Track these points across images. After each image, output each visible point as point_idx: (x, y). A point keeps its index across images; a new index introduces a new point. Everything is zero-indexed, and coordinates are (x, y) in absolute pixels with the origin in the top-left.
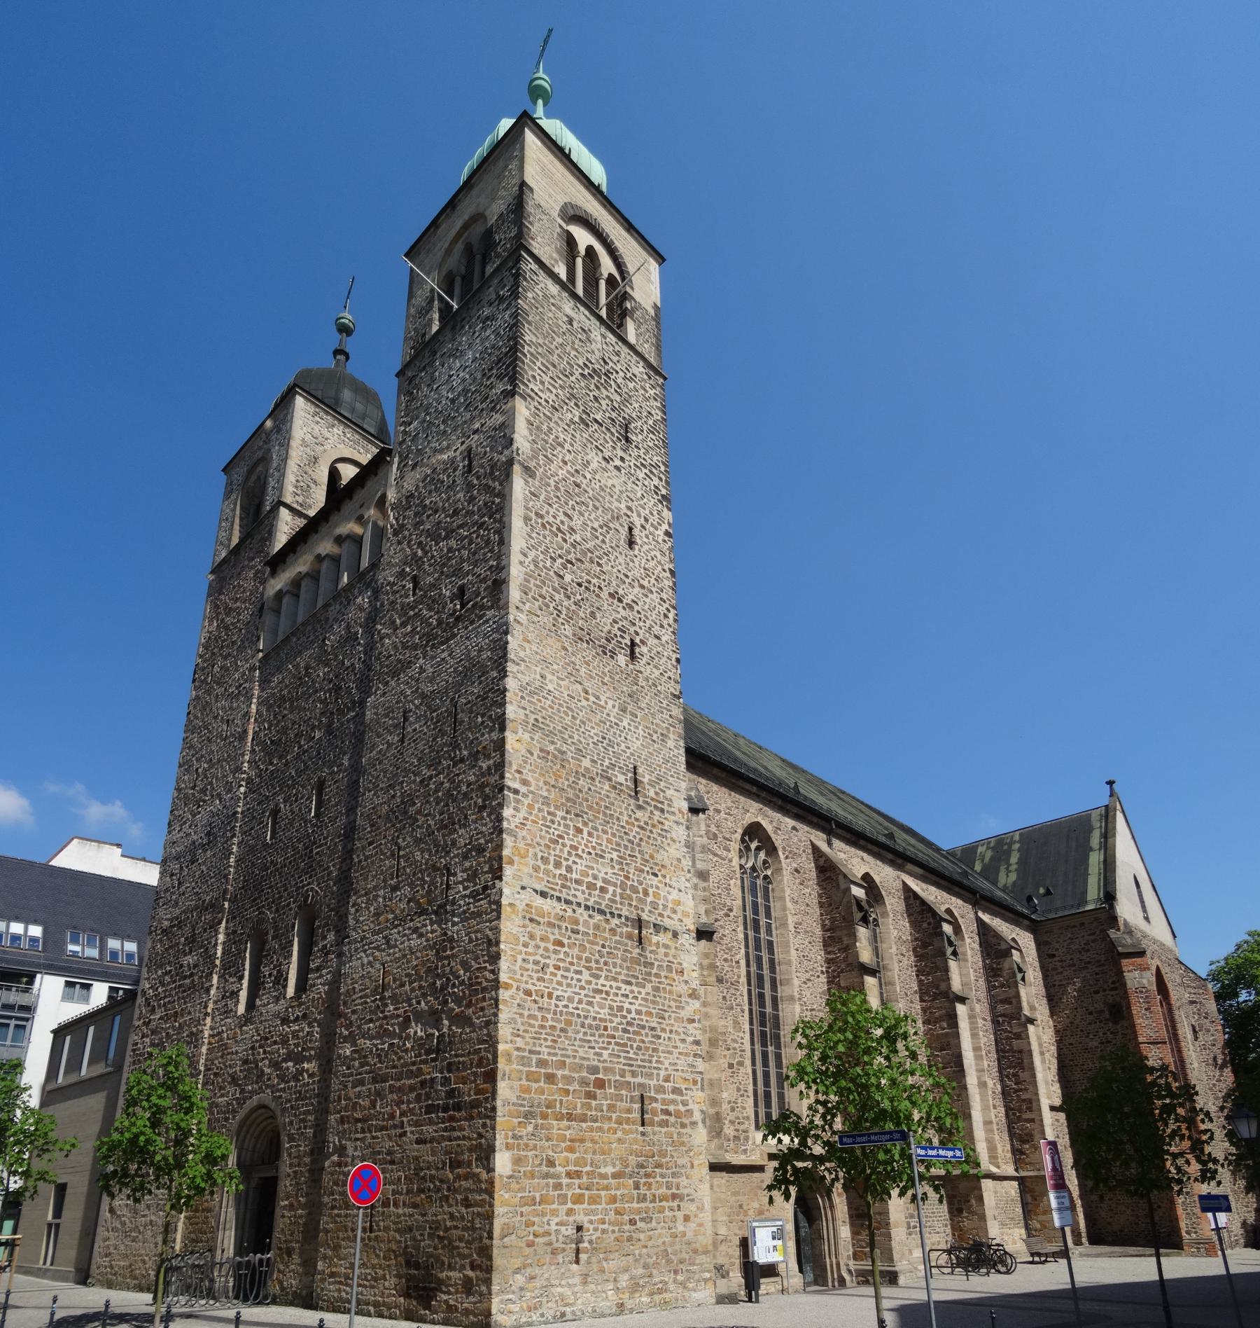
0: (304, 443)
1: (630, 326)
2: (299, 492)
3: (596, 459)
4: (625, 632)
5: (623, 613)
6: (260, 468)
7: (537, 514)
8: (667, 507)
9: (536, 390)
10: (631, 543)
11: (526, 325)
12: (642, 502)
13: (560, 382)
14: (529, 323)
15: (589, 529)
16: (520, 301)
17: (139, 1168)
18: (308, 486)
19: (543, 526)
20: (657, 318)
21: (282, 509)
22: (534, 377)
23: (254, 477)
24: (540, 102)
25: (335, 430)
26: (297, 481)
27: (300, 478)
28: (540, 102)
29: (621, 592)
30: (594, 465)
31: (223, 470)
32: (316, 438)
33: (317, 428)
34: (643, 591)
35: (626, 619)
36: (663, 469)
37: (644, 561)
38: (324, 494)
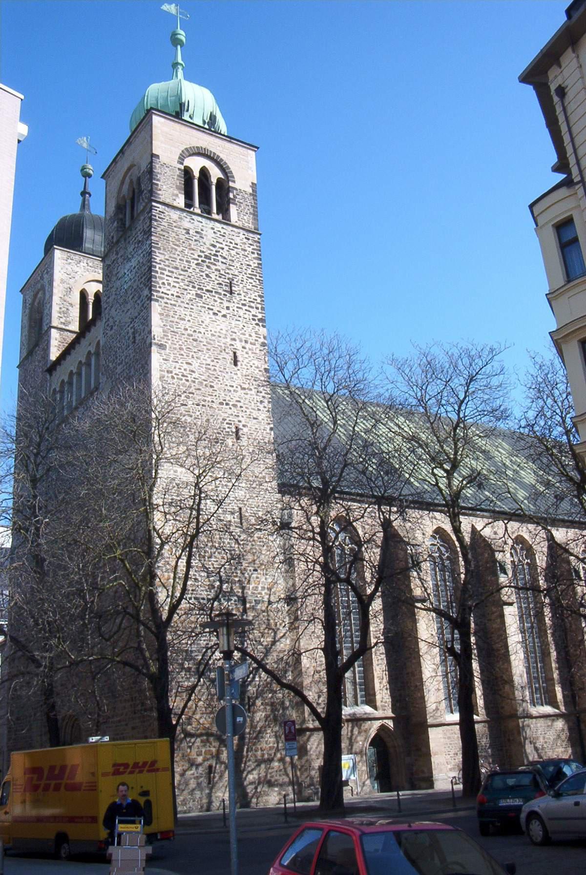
0: (62, 281)
1: (233, 209)
2: (62, 316)
3: (209, 316)
4: (231, 424)
5: (230, 412)
6: (40, 295)
7: (168, 372)
8: (263, 326)
9: (165, 291)
10: (235, 363)
11: (157, 251)
12: (243, 331)
13: (181, 277)
14: (159, 249)
15: (204, 366)
16: (153, 238)
17: (213, 604)
18: (67, 309)
19: (173, 378)
20: (254, 194)
21: (53, 330)
22: (163, 283)
23: (37, 301)
24: (179, 47)
25: (81, 263)
26: (60, 308)
27: (61, 306)
28: (179, 47)
29: (228, 398)
30: (206, 323)
31: (21, 291)
32: (70, 275)
33: (69, 267)
34: (244, 391)
35: (232, 415)
36: (259, 300)
37: (245, 370)
38: (78, 310)
